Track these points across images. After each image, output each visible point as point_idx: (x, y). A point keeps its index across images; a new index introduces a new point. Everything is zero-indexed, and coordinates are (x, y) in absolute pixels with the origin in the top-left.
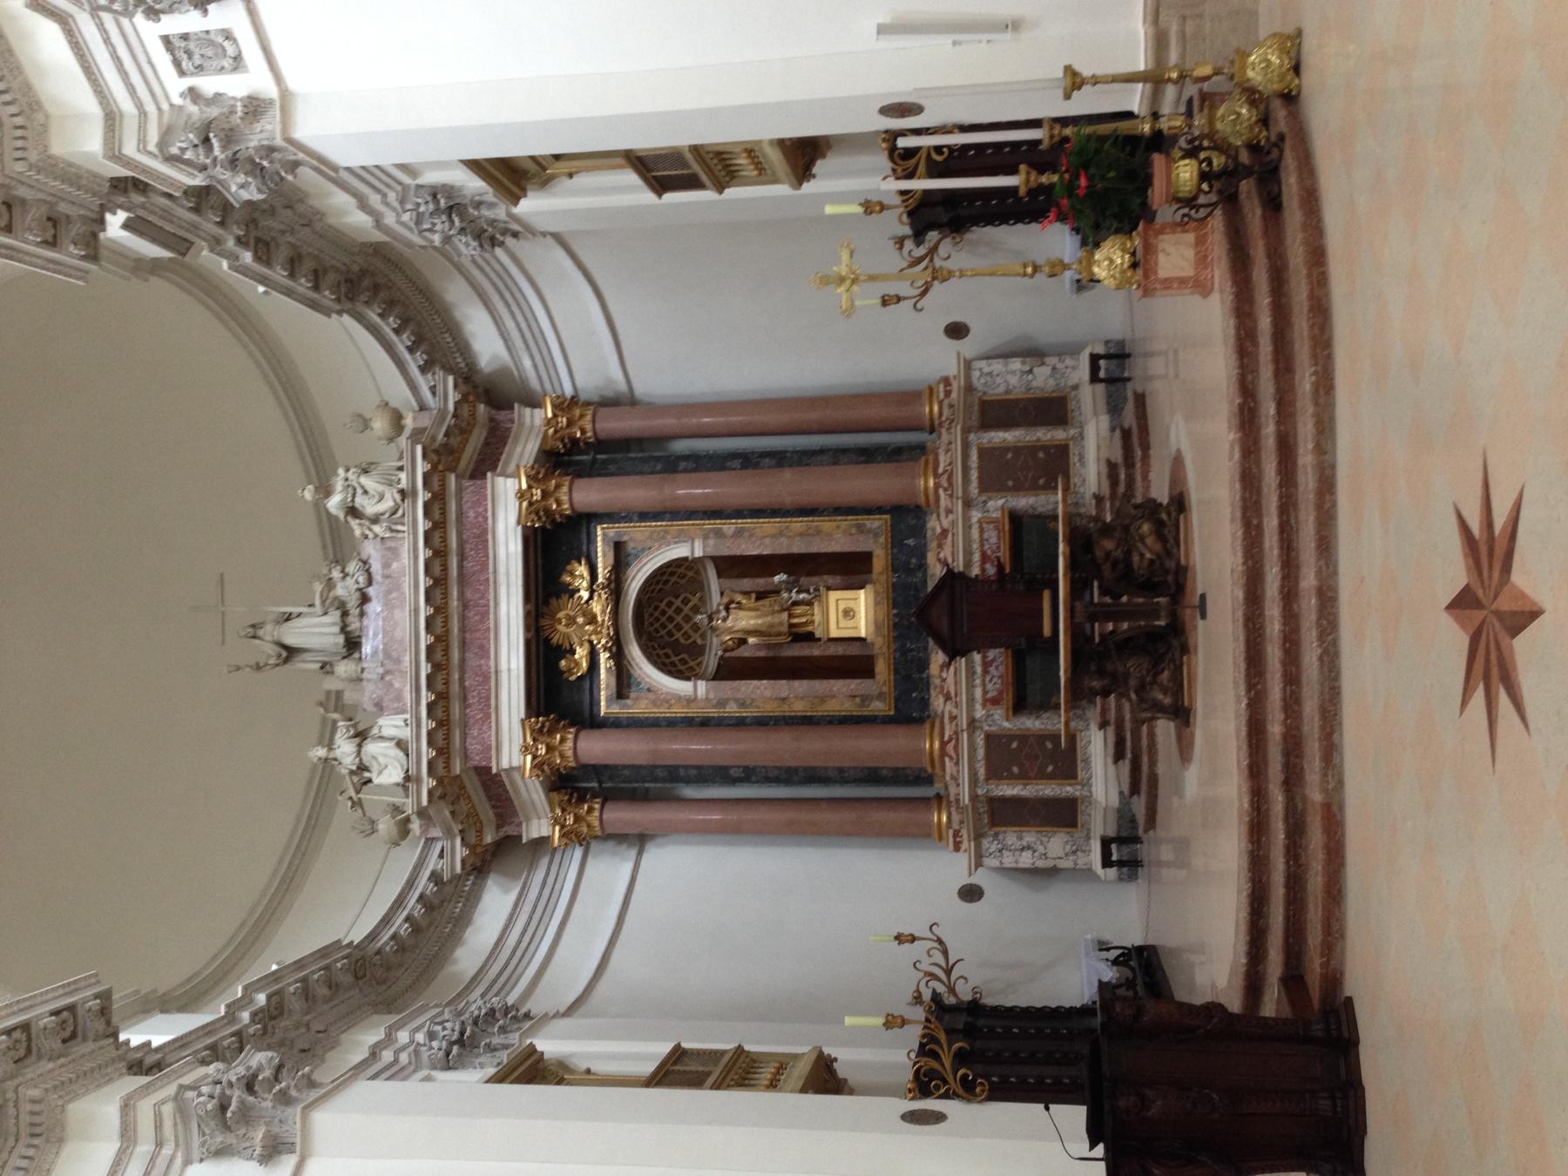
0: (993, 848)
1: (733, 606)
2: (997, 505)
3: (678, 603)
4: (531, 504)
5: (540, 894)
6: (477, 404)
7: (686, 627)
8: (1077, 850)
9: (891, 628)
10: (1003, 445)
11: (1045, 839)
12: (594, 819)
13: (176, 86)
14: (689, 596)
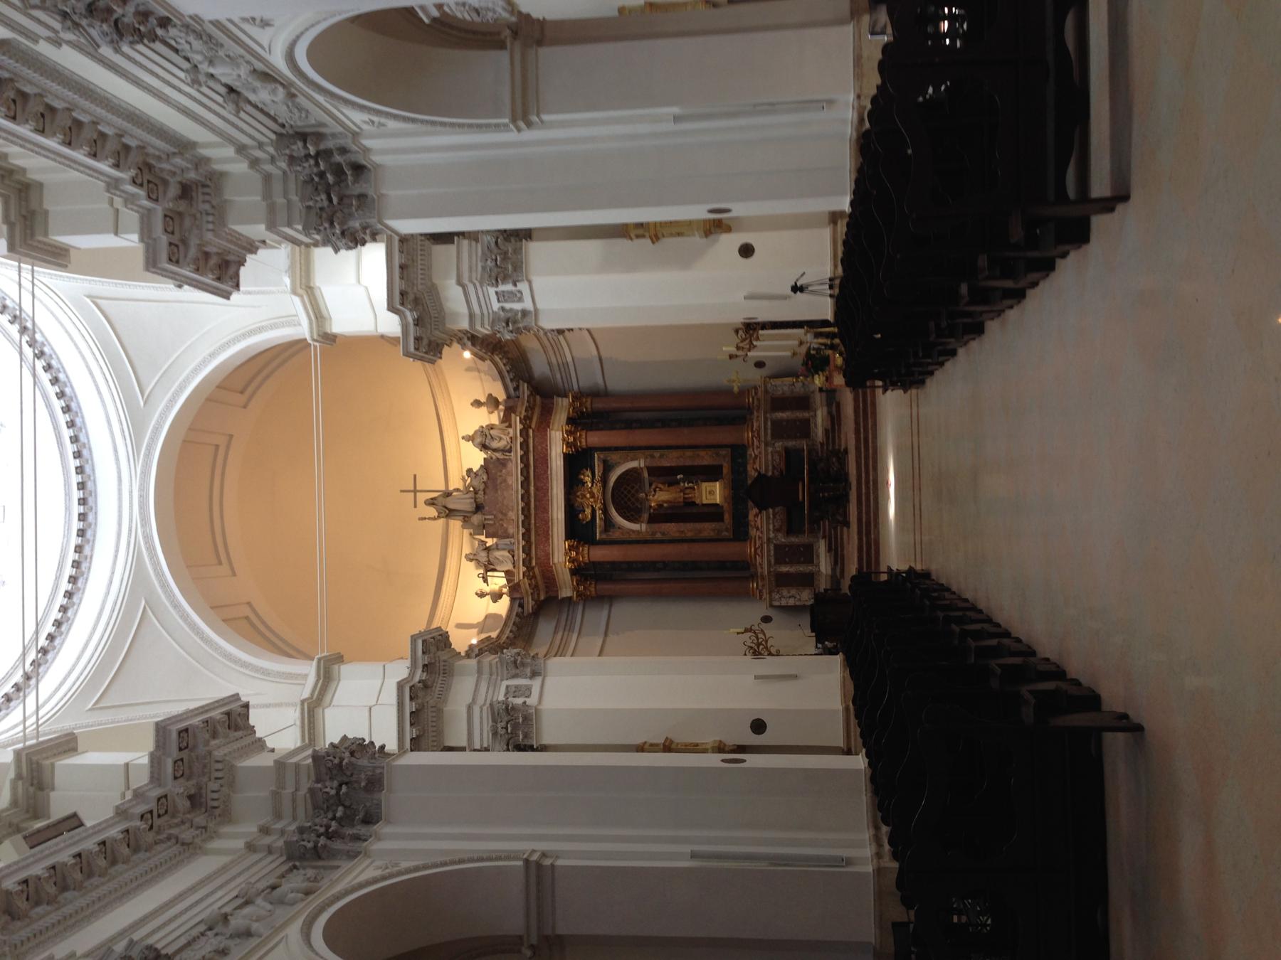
0: (777, 597)
1: (658, 489)
2: (779, 445)
3: (629, 488)
4: (568, 443)
7: (633, 500)
13: (496, 306)
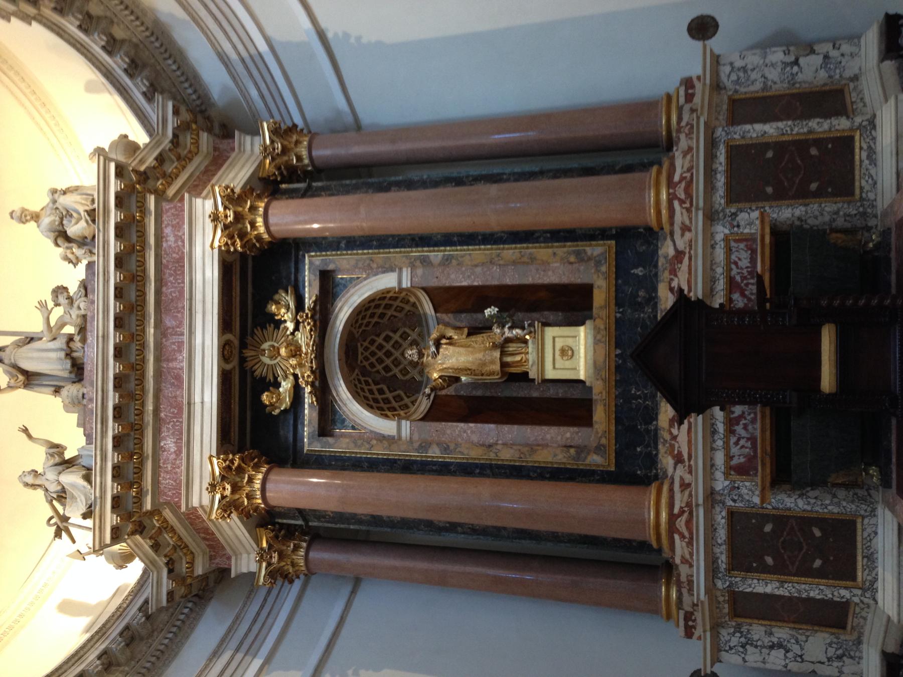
0: (734, 641)
1: (444, 341)
4: (226, 227)
5: (250, 630)
6: (201, 132)
8: (843, 655)
9: (613, 370)
12: (299, 557)
14: (408, 330)
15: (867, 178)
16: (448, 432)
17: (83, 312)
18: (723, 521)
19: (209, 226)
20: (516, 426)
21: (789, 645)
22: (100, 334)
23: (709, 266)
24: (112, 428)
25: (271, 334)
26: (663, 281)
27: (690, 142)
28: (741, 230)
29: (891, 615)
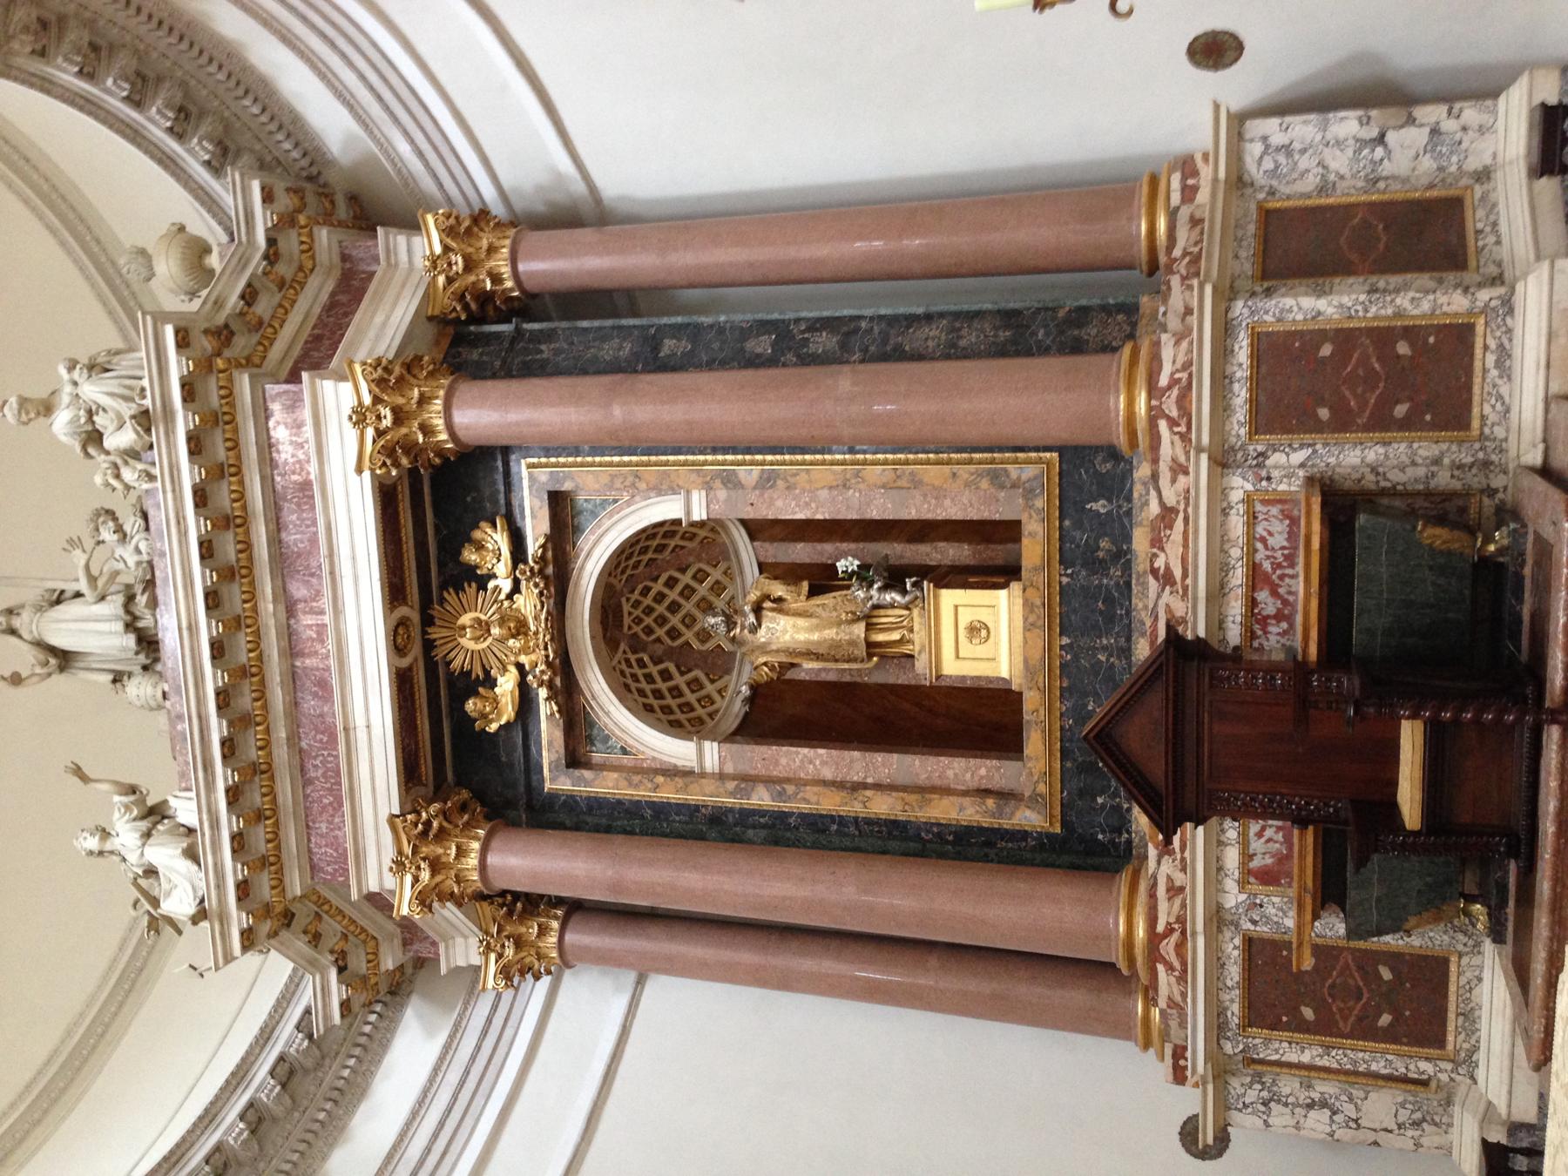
0: (1251, 1095)
3: (686, 579)
5: (478, 1048)
6: (315, 229)
10: (1311, 326)
11: (1357, 1093)
15: (1493, 401)
16: (783, 761)
17: (145, 557)
18: (1236, 953)
19: (352, 434)
20: (895, 756)
21: (1337, 1104)
22: (184, 624)
23: (1218, 540)
24: (222, 777)
25: (473, 600)
26: (1141, 524)
27: (1187, 293)
28: (1274, 486)
29: (1495, 1101)
